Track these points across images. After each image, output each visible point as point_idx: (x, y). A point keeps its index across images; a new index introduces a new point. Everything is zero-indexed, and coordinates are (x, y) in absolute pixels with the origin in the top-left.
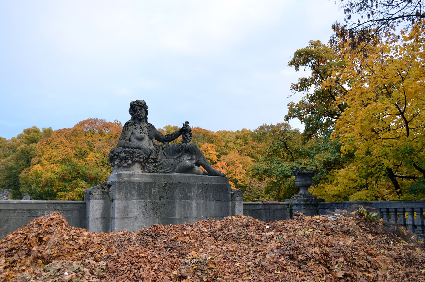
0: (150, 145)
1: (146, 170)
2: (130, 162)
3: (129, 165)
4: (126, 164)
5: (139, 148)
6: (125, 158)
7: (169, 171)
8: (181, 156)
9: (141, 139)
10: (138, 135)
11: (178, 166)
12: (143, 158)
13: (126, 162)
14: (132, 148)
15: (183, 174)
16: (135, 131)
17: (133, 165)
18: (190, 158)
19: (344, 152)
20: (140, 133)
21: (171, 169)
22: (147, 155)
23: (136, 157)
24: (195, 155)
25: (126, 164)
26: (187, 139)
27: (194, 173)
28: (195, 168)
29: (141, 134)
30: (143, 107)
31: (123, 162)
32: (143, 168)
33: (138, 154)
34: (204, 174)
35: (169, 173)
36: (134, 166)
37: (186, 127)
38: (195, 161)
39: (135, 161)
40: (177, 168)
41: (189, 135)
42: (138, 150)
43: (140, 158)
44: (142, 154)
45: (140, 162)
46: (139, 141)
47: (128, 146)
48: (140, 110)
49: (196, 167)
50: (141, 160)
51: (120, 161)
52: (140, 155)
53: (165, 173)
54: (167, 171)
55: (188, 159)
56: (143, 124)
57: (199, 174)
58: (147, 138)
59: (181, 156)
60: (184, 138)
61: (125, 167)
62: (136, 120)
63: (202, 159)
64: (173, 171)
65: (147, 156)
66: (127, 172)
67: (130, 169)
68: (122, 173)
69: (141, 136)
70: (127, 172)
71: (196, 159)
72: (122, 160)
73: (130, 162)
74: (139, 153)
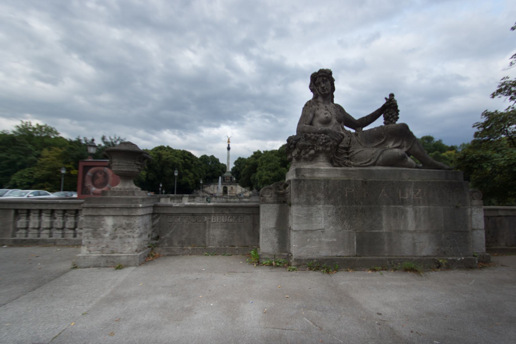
1: (335, 164)
2: (312, 152)
8: (383, 143)
20: (326, 114)
21: (370, 161)
26: (391, 119)
29: (327, 115)
31: (303, 152)
33: (324, 141)
43: (327, 146)
48: (324, 81)
54: (365, 163)
55: (395, 146)
58: (334, 121)
64: (374, 164)
68: (302, 167)
69: (327, 117)
74: (325, 139)
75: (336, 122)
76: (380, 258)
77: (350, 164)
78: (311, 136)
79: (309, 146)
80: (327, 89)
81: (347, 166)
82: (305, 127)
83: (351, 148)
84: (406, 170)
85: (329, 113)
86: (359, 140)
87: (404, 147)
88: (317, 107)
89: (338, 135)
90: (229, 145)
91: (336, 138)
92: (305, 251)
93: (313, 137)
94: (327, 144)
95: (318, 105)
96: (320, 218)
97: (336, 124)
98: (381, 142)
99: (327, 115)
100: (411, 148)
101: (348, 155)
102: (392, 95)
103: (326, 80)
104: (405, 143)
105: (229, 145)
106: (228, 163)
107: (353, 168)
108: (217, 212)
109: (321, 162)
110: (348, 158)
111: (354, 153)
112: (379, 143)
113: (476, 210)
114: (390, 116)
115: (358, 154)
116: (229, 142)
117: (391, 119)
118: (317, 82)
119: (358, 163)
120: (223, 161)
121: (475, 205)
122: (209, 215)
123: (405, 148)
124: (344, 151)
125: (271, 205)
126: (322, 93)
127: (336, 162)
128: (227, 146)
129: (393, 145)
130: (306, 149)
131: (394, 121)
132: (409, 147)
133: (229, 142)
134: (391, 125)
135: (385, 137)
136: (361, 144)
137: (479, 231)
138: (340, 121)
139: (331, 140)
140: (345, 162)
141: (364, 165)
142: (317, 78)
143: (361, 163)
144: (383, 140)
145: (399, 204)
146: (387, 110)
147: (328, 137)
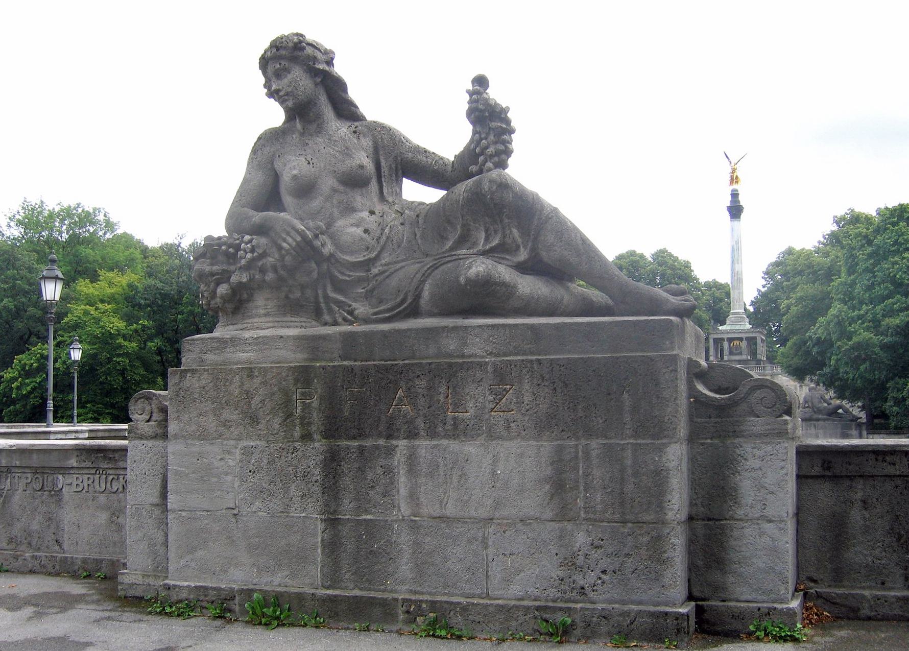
33: (249, 256)
74: (252, 250)
75: (336, 184)
76: (379, 595)
90: (735, 195)
92: (193, 564)
96: (229, 478)
97: (335, 191)
102: (481, 82)
105: (735, 195)
106: (737, 277)
108: (83, 465)
116: (734, 180)
120: (708, 269)
121: (759, 436)
122: (65, 470)
123: (522, 249)
125: (150, 443)
128: (727, 201)
133: (734, 180)
137: (767, 526)
145: (447, 436)
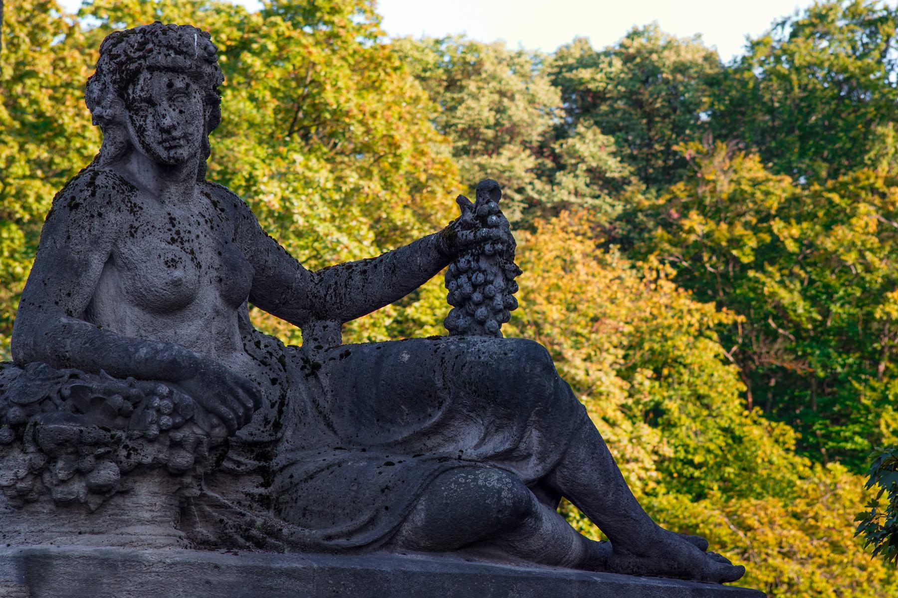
0: (227, 347)
1: (203, 530)
2: (108, 473)
3: (103, 492)
4: (78, 488)
5: (173, 371)
6: (76, 446)
7: (357, 540)
8: (437, 429)
9: (173, 305)
10: (157, 277)
11: (421, 505)
12: (199, 443)
13: (80, 473)
14: (121, 375)
15: (453, 562)
16: (132, 250)
17: (124, 493)
18: (498, 443)
19: (811, 514)
20: (172, 263)
21: (372, 521)
22: (223, 420)
23: (151, 441)
24: (545, 431)
25: (78, 488)
26: (481, 312)
27: (528, 556)
28: (538, 519)
29: (178, 273)
30: (197, 77)
31: (61, 469)
32: (184, 513)
33: (165, 420)
34: (591, 559)
35: (358, 549)
36: (128, 502)
37: (483, 219)
38: (531, 470)
39: (140, 465)
40: (419, 517)
41: (500, 282)
42: (164, 389)
43: (176, 445)
44: (191, 421)
45: (174, 474)
46: (159, 321)
47: (321, 419)
48: (173, 94)
49: (541, 508)
50: (183, 458)
51: (40, 461)
52: (176, 427)
53: (335, 551)
54: (349, 534)
55: (489, 448)
56: (187, 195)
57: (555, 562)
58: (210, 298)
59: (437, 429)
60: (458, 301)
61: (66, 505)
62: (140, 170)
63: (582, 453)
64: (388, 542)
65: (220, 432)
66: (82, 546)
67: (101, 522)
68: (53, 549)
69: (177, 283)
70: (82, 546)
71: (542, 458)
72: (52, 459)
73: (108, 473)
74: (174, 412)
75: (219, 302)
77: (275, 534)
78: (109, 393)
79: (97, 444)
80: (185, 136)
81: (260, 545)
82: (67, 329)
83: (282, 447)
84: (527, 579)
85: (186, 258)
86: (326, 404)
87: (529, 455)
88: (125, 218)
89: (231, 391)
91: (223, 409)
93: (118, 400)
94: (178, 435)
95: (134, 209)
98: (429, 423)
99: (178, 273)
100: (559, 464)
101: (266, 485)
103: (186, 92)
104: (534, 436)
107: (290, 561)
109: (141, 522)
110: (265, 502)
111: (298, 472)
112: (417, 428)
113: (586, 124)
114: (477, 297)
115: (317, 482)
117: (481, 312)
118: (137, 91)
119: (315, 534)
123: (533, 460)
124: (250, 463)
126: (164, 154)
127: (206, 518)
129: (482, 441)
130: (78, 455)
131: (492, 323)
132: (554, 458)
134: (478, 342)
135: (448, 401)
136: (329, 425)
138: (234, 300)
139: (200, 417)
140: (252, 524)
141: (343, 542)
142: (138, 71)
143: (329, 531)
144: (437, 416)
146: (462, 263)
147: (188, 399)
